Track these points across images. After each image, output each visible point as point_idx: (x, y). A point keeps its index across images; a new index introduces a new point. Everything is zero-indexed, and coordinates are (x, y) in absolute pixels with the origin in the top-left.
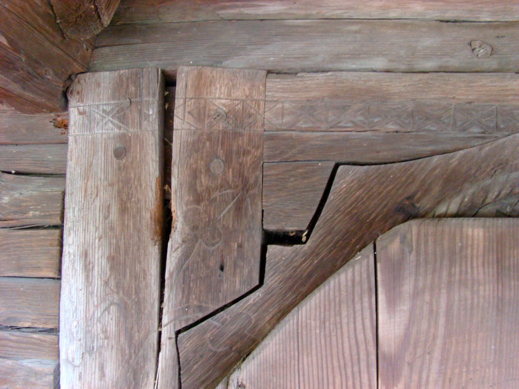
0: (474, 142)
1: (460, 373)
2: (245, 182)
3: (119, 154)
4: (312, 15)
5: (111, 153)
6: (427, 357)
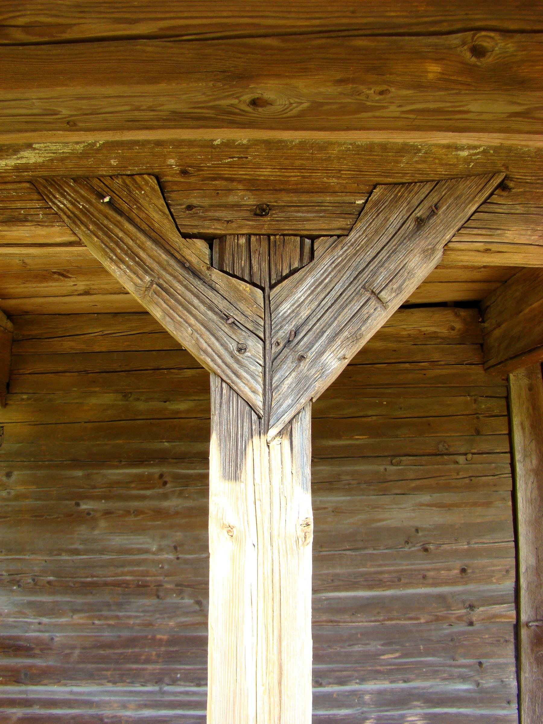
3: (530, 389)
5: (527, 390)
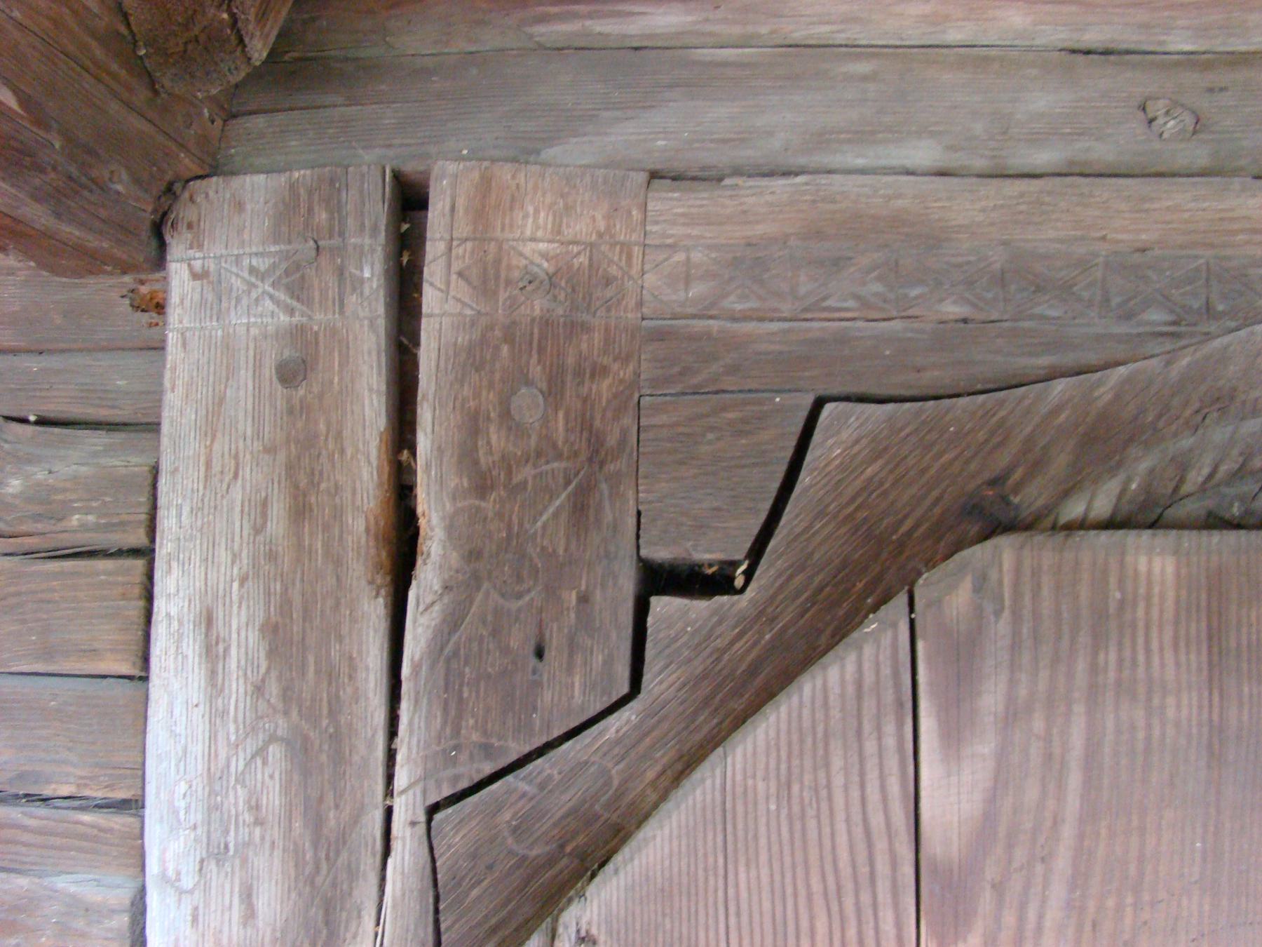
0: (1153, 347)
1: (1119, 908)
2: (596, 443)
3: (290, 374)
4: (760, 36)
5: (269, 371)
6: (1039, 868)
